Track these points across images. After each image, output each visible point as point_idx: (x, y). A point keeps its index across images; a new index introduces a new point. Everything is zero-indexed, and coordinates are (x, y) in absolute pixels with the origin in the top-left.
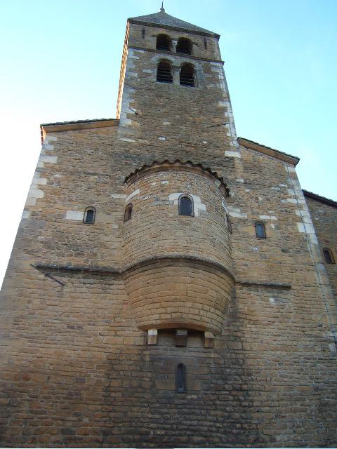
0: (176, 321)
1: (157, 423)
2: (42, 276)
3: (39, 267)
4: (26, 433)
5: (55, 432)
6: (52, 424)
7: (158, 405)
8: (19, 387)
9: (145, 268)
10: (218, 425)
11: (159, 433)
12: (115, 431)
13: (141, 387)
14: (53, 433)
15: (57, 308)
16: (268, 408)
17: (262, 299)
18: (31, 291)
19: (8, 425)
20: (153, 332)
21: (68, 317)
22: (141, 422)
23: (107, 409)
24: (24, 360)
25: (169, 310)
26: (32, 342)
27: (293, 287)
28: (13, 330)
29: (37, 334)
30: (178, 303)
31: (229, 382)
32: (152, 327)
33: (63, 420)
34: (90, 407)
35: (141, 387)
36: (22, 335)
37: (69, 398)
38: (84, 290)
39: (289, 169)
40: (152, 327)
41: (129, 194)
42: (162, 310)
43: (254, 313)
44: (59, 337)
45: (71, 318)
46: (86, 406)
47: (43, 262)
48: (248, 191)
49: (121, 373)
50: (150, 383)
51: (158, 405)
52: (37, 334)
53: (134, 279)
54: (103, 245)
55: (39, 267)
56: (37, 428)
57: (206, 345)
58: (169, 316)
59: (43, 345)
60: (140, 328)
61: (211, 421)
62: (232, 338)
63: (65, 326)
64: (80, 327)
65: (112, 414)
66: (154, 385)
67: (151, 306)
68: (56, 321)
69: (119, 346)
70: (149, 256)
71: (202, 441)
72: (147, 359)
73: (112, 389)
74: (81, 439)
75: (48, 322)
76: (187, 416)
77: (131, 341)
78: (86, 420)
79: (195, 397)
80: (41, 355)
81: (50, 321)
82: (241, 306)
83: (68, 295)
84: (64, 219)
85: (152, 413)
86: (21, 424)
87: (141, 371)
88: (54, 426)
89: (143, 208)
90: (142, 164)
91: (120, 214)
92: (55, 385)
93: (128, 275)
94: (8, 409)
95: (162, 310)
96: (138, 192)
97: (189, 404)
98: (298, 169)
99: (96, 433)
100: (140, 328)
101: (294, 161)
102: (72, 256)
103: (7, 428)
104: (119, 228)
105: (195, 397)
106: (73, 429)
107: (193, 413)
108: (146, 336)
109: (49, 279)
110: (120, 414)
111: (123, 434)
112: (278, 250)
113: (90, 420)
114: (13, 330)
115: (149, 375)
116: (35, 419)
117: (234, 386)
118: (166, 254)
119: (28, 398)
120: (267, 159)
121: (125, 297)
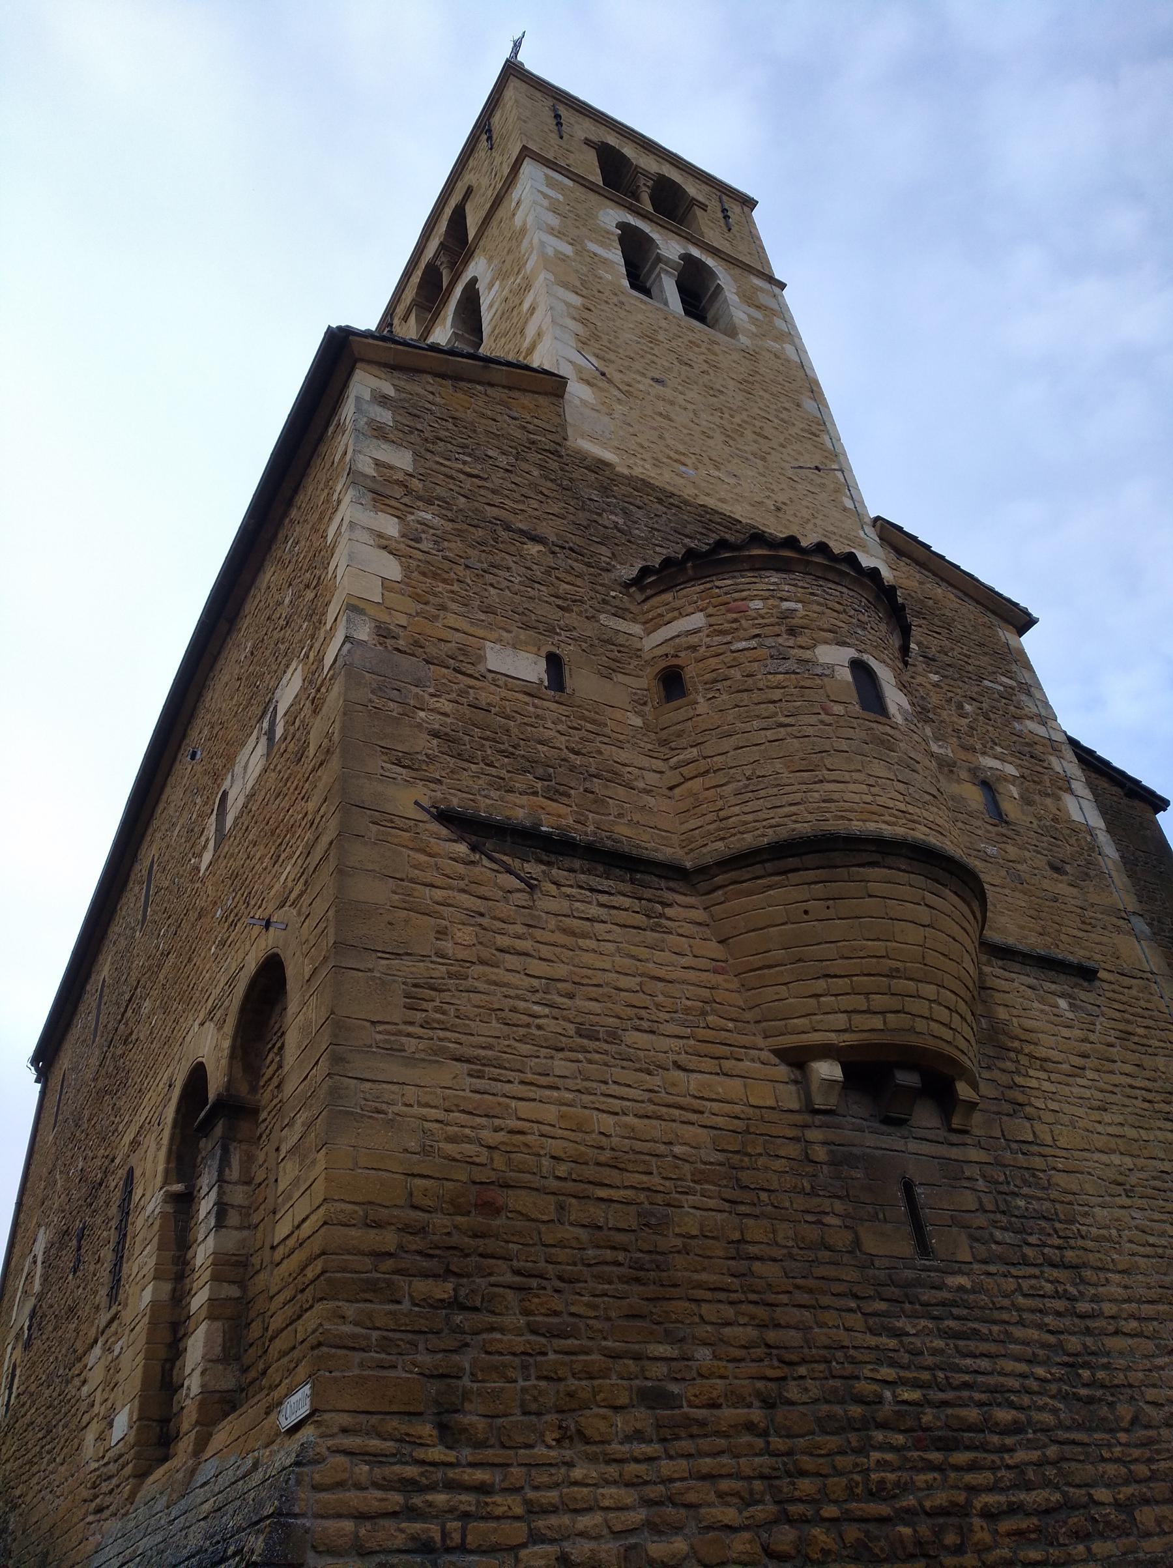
0: (899, 1039)
1: (893, 1364)
2: (462, 849)
3: (446, 817)
4: (534, 1407)
5: (623, 1400)
6: (604, 1374)
7: (882, 1306)
8: (475, 1236)
9: (792, 862)
10: (1040, 1371)
11: (906, 1396)
12: (793, 1391)
13: (828, 1248)
14: (619, 1402)
15: (536, 967)
16: (1134, 1324)
17: (1042, 1001)
18: (439, 894)
19: (466, 1381)
20: (827, 1070)
21: (571, 996)
22: (854, 1362)
23: (753, 1317)
24: (469, 1140)
25: (878, 1001)
26: (480, 1075)
27: (1102, 974)
28: (410, 1029)
29: (490, 1047)
30: (900, 985)
31: (1033, 1239)
32: (825, 1052)
33: (637, 1357)
34: (705, 1308)
35: (828, 1248)
36: (442, 1051)
37: (637, 1280)
38: (594, 911)
39: (1006, 635)
40: (825, 1052)
41: (652, 625)
42: (860, 1002)
43: (1033, 1036)
44: (560, 1065)
45: (579, 1002)
46: (693, 1306)
47: (455, 802)
48: (936, 678)
49: (764, 1196)
50: (849, 1236)
51: (882, 1306)
52: (490, 1047)
53: (751, 893)
54: (613, 776)
55: (446, 817)
56: (561, 1386)
57: (956, 1122)
58: (877, 1022)
59: (516, 1089)
60: (783, 1054)
61: (1018, 1359)
62: (1008, 1107)
63: (571, 1029)
64: (614, 1037)
65: (772, 1336)
66: (857, 1242)
67: (821, 985)
68: (536, 1008)
69: (737, 1109)
70: (804, 828)
71: (1015, 1422)
72: (821, 1153)
73: (753, 1250)
74: (702, 1424)
75: (514, 1010)
76: (961, 1343)
77: (763, 1095)
78: (703, 1354)
79: (962, 1280)
80: (520, 1125)
81: (522, 1005)
82: (1002, 1013)
83: (552, 923)
84: (481, 668)
85: (872, 1332)
86: (511, 1374)
87: (813, 1193)
88: (614, 1380)
89: (736, 673)
90: (713, 538)
91: (645, 681)
92: (583, 1234)
93: (719, 880)
94: (458, 1319)
95: (860, 1002)
96: (697, 620)
97: (954, 1304)
98: (1030, 642)
99: (740, 1401)
100: (783, 1054)
101: (1023, 621)
102: (535, 794)
103: (466, 1395)
104: (647, 726)
105: (962, 1280)
106: (675, 1388)
107: (975, 1334)
108: (802, 1081)
109: (486, 862)
110: (792, 1332)
111: (815, 1401)
112: (1041, 861)
113: (716, 1357)
114: (410, 1029)
115: (839, 1206)
116: (552, 1356)
117: (1046, 1250)
118: (857, 826)
119: (509, 1278)
120: (952, 597)
121: (713, 949)
